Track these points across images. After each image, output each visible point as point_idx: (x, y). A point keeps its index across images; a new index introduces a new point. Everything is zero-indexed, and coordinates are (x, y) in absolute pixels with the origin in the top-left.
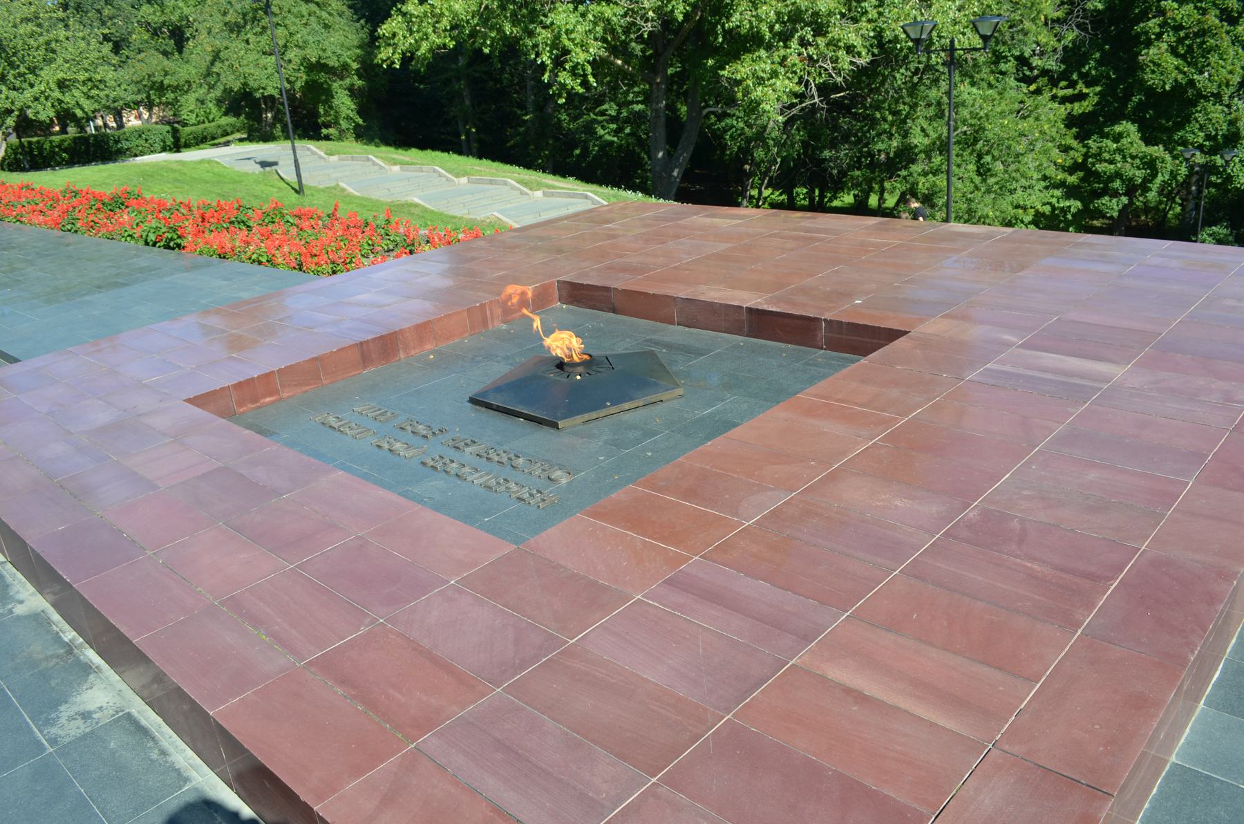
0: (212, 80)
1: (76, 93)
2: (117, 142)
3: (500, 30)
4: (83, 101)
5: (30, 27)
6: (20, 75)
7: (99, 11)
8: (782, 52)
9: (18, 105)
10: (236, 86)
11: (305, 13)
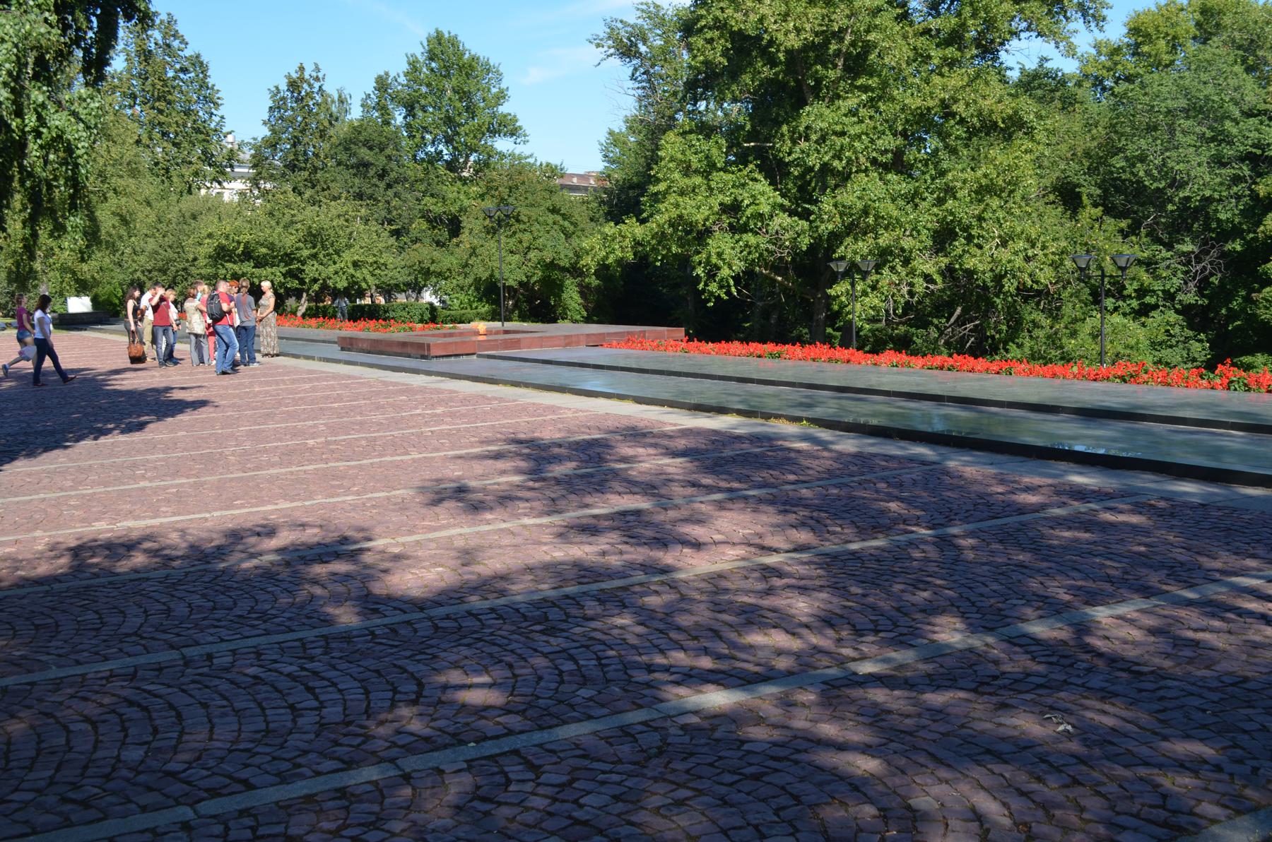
0: (467, 270)
1: (365, 271)
2: (386, 312)
3: (669, 250)
4: (369, 277)
5: (342, 222)
6: (328, 255)
7: (388, 202)
8: (874, 277)
9: (324, 276)
10: (485, 276)
11: (550, 222)
